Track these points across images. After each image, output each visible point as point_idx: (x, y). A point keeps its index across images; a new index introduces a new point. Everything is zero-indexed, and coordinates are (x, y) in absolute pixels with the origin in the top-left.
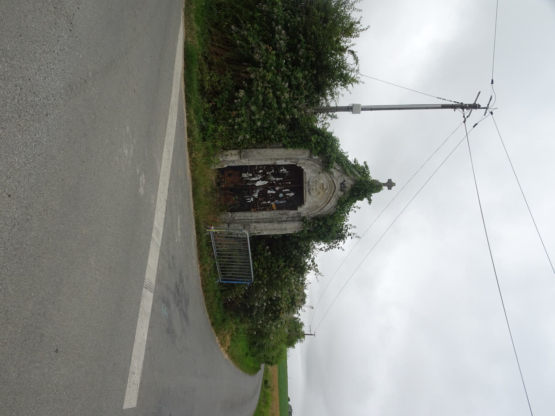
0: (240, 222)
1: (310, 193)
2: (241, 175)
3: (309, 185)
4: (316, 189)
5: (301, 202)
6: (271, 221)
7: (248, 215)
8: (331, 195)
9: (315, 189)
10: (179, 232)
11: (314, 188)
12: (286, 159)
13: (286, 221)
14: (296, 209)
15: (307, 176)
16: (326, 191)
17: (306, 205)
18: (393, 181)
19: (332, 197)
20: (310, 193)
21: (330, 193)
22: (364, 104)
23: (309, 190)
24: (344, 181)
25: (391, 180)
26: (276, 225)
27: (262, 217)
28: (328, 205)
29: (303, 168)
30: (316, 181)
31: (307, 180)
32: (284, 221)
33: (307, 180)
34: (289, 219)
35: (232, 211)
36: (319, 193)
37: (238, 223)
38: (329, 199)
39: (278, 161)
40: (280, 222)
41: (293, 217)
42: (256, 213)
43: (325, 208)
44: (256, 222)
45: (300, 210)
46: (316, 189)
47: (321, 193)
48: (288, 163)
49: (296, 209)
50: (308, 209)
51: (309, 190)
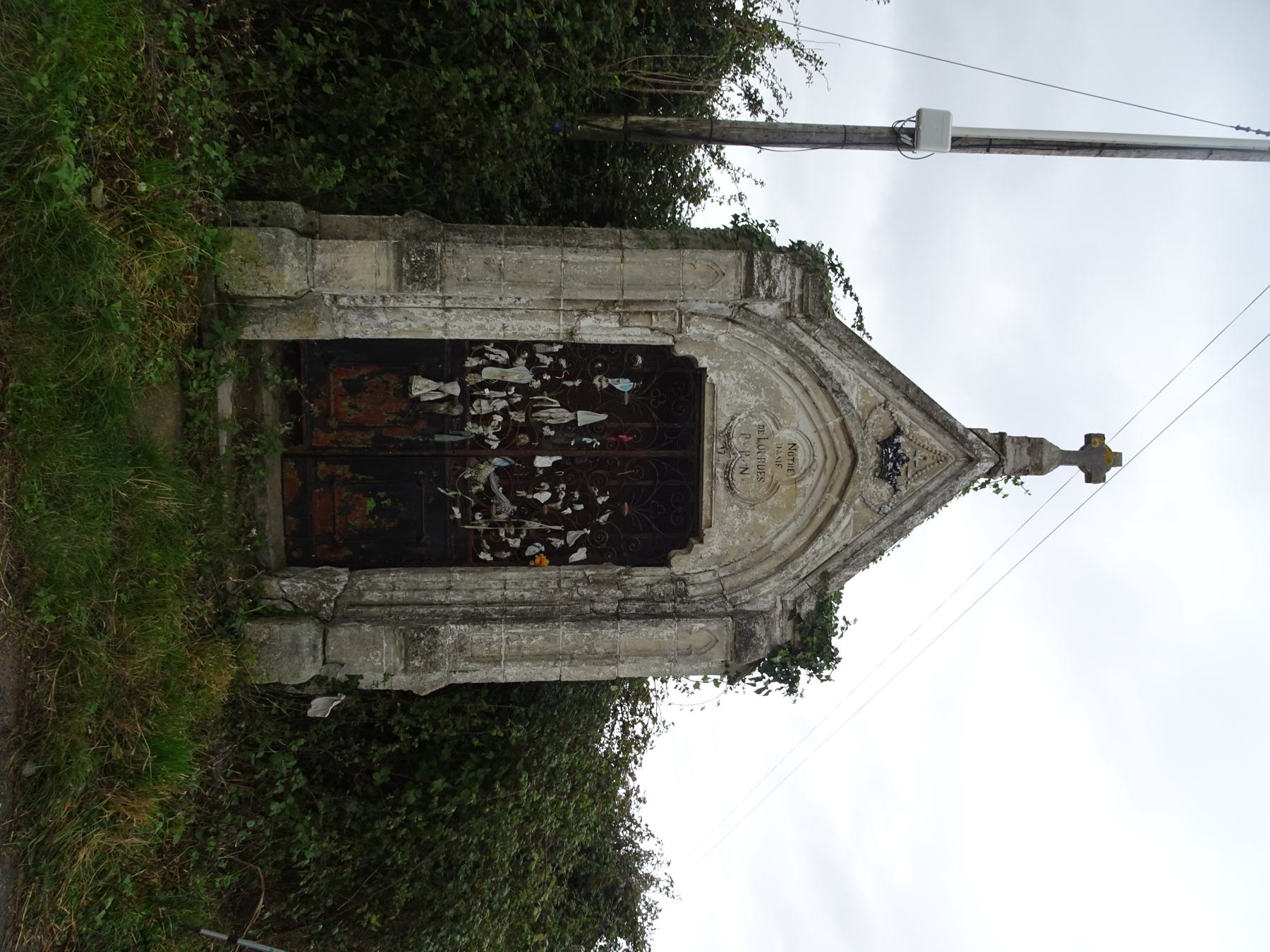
0: (389, 615)
1: (730, 487)
2: (407, 385)
3: (727, 447)
4: (761, 470)
5: (687, 529)
6: (541, 614)
7: (432, 581)
8: (833, 499)
9: (753, 469)
10: (617, 124)
11: (752, 462)
12: (624, 309)
13: (617, 616)
14: (666, 563)
15: (722, 403)
16: (809, 481)
17: (714, 543)
18: (1113, 445)
19: (835, 509)
20: (730, 487)
21: (828, 488)
22: (966, 120)
23: (728, 470)
24: (898, 431)
25: (1089, 479)
26: (566, 635)
27: (497, 595)
28: (818, 545)
29: (703, 362)
30: (761, 428)
31: (721, 425)
32: (603, 617)
33: (721, 425)
34: (632, 607)
35: (356, 564)
36: (774, 488)
37: (375, 621)
38: (821, 515)
39: (587, 322)
40: (586, 618)
41: (650, 599)
42: (470, 577)
43: (802, 560)
44: (467, 618)
45: (682, 563)
46: (761, 470)
47: (783, 489)
48: (636, 334)
49: (666, 563)
50: (718, 559)
51: (728, 470)
